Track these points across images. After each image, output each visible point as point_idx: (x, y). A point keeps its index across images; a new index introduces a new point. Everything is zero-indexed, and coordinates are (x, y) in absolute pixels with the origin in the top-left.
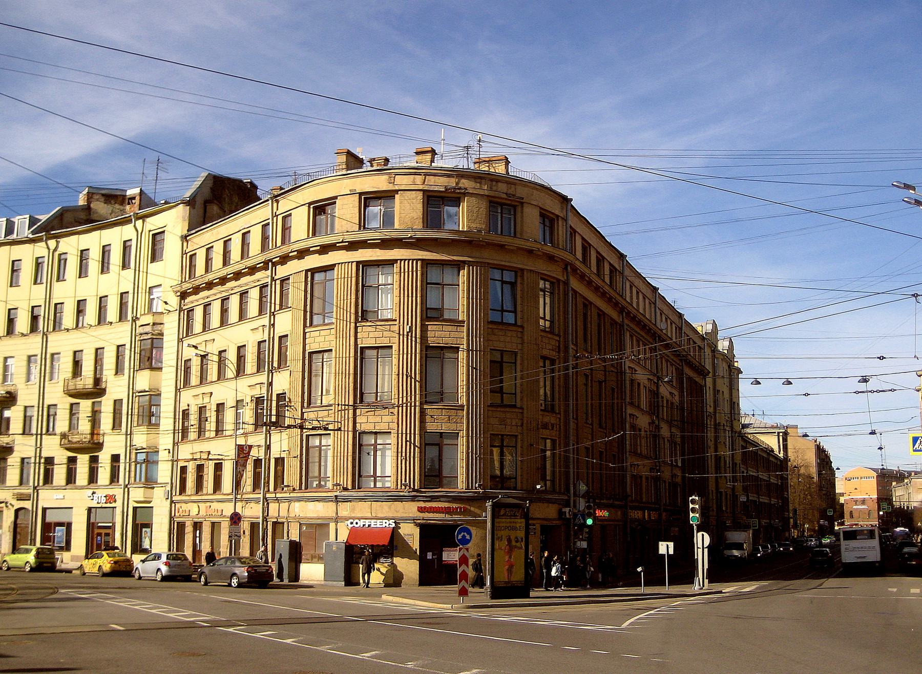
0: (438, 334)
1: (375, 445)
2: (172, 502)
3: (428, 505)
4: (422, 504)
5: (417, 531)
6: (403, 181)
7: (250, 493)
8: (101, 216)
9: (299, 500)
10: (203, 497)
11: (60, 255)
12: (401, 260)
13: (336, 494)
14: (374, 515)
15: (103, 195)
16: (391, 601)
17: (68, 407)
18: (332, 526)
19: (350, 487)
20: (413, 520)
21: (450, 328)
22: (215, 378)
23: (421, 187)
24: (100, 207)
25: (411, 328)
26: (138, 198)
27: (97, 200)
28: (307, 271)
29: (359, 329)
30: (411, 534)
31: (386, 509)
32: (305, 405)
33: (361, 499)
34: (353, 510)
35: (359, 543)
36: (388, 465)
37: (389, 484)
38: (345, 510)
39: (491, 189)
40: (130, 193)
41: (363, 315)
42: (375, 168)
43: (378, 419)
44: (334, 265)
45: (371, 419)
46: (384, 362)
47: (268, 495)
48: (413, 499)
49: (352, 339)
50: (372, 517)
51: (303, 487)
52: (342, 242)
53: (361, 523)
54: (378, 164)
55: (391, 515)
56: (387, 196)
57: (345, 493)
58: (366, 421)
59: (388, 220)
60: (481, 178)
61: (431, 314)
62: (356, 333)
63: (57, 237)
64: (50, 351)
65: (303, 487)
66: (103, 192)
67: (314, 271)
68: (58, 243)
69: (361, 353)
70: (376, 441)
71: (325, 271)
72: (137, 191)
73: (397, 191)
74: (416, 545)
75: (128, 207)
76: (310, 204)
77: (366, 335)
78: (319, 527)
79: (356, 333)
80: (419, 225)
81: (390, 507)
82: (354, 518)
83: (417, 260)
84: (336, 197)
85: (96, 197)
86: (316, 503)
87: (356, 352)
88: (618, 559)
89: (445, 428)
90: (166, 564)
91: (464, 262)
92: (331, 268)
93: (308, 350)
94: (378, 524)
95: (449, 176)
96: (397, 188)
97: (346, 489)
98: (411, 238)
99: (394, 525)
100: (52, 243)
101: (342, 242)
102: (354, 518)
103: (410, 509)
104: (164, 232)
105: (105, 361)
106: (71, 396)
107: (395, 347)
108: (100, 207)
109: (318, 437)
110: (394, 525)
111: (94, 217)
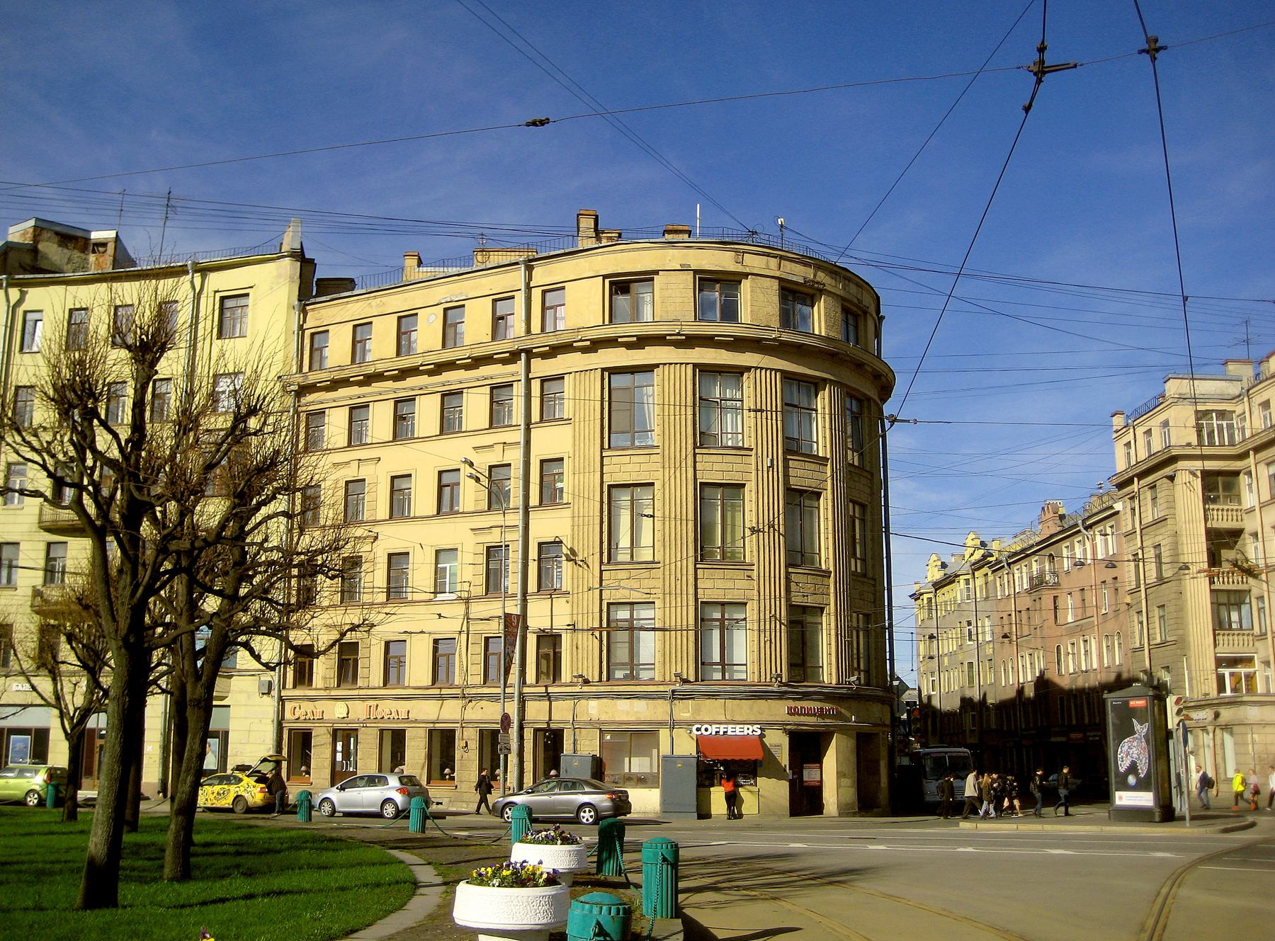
0: (802, 475)
1: (722, 620)
2: (281, 700)
3: (799, 704)
4: (792, 704)
5: (785, 741)
6: (754, 263)
7: (379, 688)
8: (53, 264)
9: (598, 696)
10: (362, 692)
11: (25, 312)
12: (756, 368)
13: (673, 688)
14: (729, 718)
15: (57, 233)
16: (801, 840)
17: (43, 546)
18: (664, 734)
19: (692, 678)
20: (782, 725)
21: (813, 466)
22: (383, 511)
23: (777, 274)
24: (51, 250)
25: (772, 461)
26: (111, 247)
27: (49, 240)
28: (603, 370)
29: (699, 458)
30: (779, 743)
31: (746, 709)
32: (605, 560)
33: (712, 696)
34: (697, 710)
35: (711, 756)
36: (751, 650)
37: (752, 677)
38: (684, 710)
39: (844, 288)
40: (96, 236)
41: (703, 439)
42: (604, 242)
43: (730, 584)
44: (657, 366)
45: (719, 584)
46: (733, 506)
47: (526, 690)
48: (781, 696)
49: (691, 471)
50: (736, 722)
51: (604, 678)
52: (678, 334)
53: (713, 729)
54: (610, 238)
55: (753, 718)
56: (730, 281)
57: (687, 687)
58: (716, 585)
59: (730, 313)
60: (836, 273)
61: (794, 447)
62: (695, 462)
63: (22, 285)
64: (537, 455)
65: (604, 678)
66: (57, 229)
67: (613, 371)
68: (23, 294)
69: (703, 488)
70: (632, 615)
71: (632, 373)
72: (112, 234)
73: (746, 275)
74: (784, 759)
75: (92, 258)
76: (605, 277)
77: (708, 466)
78: (641, 737)
79: (695, 462)
80: (775, 323)
81: (751, 709)
82: (702, 723)
83: (777, 371)
84: (657, 272)
85: (46, 235)
86: (635, 701)
87: (695, 489)
88: (699, 773)
89: (811, 601)
90: (401, 791)
91: (825, 380)
92: (649, 368)
93: (608, 480)
94: (738, 730)
95: (805, 264)
96: (748, 270)
97: (686, 681)
98: (774, 340)
99: (759, 732)
100: (14, 293)
101: (581, 340)
102: (702, 723)
103: (778, 710)
104: (247, 295)
105: (532, 480)
106: (49, 530)
107: (658, 485)
108: (51, 250)
109: (628, 607)
110: (759, 732)
111: (43, 265)
